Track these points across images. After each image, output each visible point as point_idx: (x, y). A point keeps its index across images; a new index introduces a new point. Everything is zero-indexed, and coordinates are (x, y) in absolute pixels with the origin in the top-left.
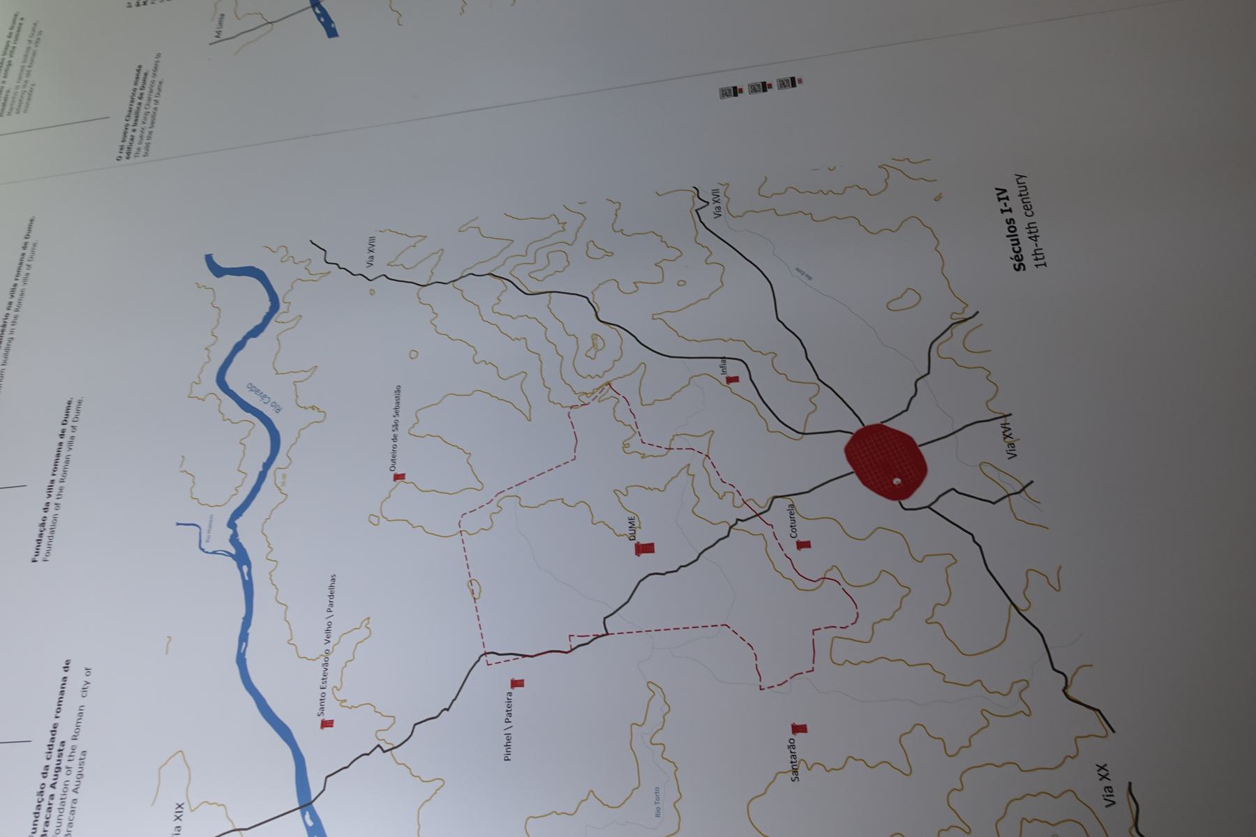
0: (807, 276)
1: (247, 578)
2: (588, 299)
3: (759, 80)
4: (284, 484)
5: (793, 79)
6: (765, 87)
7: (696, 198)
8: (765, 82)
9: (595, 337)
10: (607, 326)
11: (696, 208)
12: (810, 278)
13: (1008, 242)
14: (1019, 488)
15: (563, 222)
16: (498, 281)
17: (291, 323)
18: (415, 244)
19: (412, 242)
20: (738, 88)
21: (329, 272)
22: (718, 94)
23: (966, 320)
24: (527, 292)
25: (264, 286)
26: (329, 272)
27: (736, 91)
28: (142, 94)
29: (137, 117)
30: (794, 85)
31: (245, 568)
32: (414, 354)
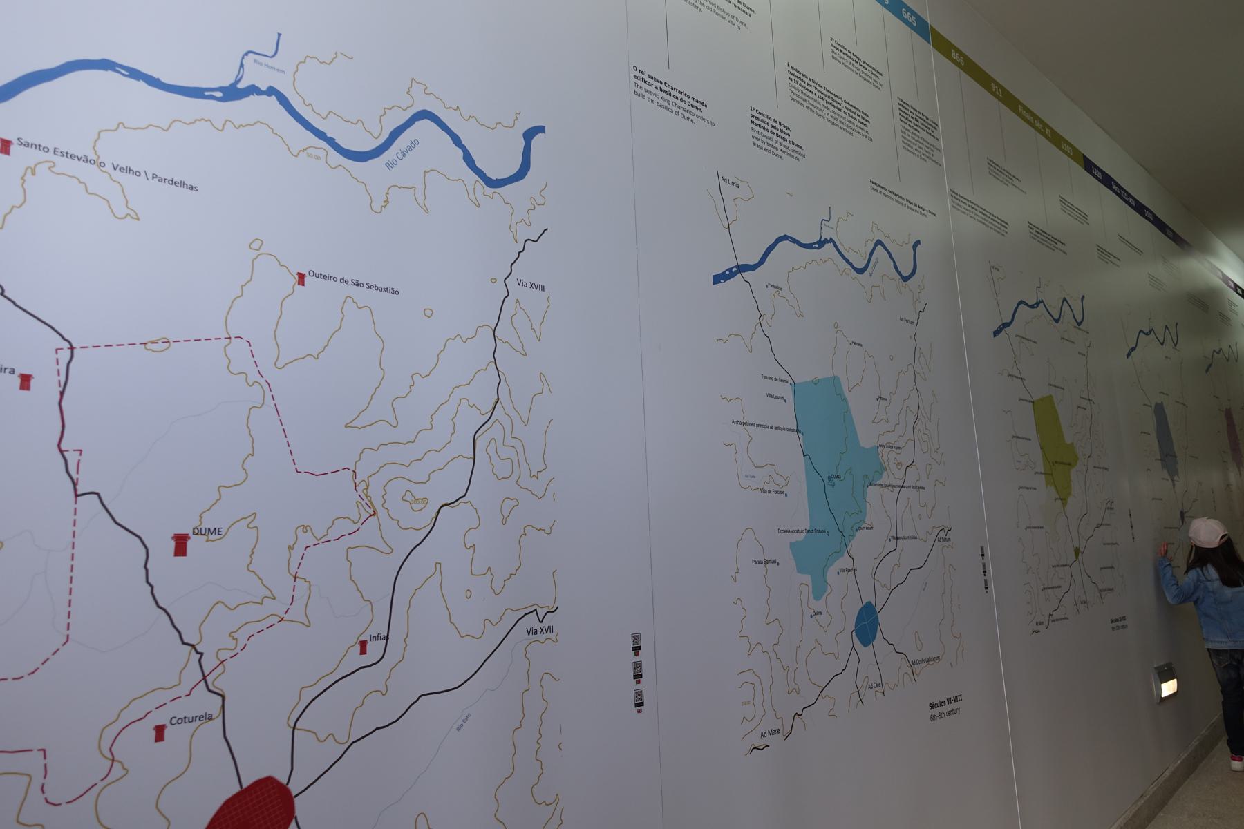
1: (206, 93)
4: (310, 155)
7: (547, 610)
9: (425, 501)
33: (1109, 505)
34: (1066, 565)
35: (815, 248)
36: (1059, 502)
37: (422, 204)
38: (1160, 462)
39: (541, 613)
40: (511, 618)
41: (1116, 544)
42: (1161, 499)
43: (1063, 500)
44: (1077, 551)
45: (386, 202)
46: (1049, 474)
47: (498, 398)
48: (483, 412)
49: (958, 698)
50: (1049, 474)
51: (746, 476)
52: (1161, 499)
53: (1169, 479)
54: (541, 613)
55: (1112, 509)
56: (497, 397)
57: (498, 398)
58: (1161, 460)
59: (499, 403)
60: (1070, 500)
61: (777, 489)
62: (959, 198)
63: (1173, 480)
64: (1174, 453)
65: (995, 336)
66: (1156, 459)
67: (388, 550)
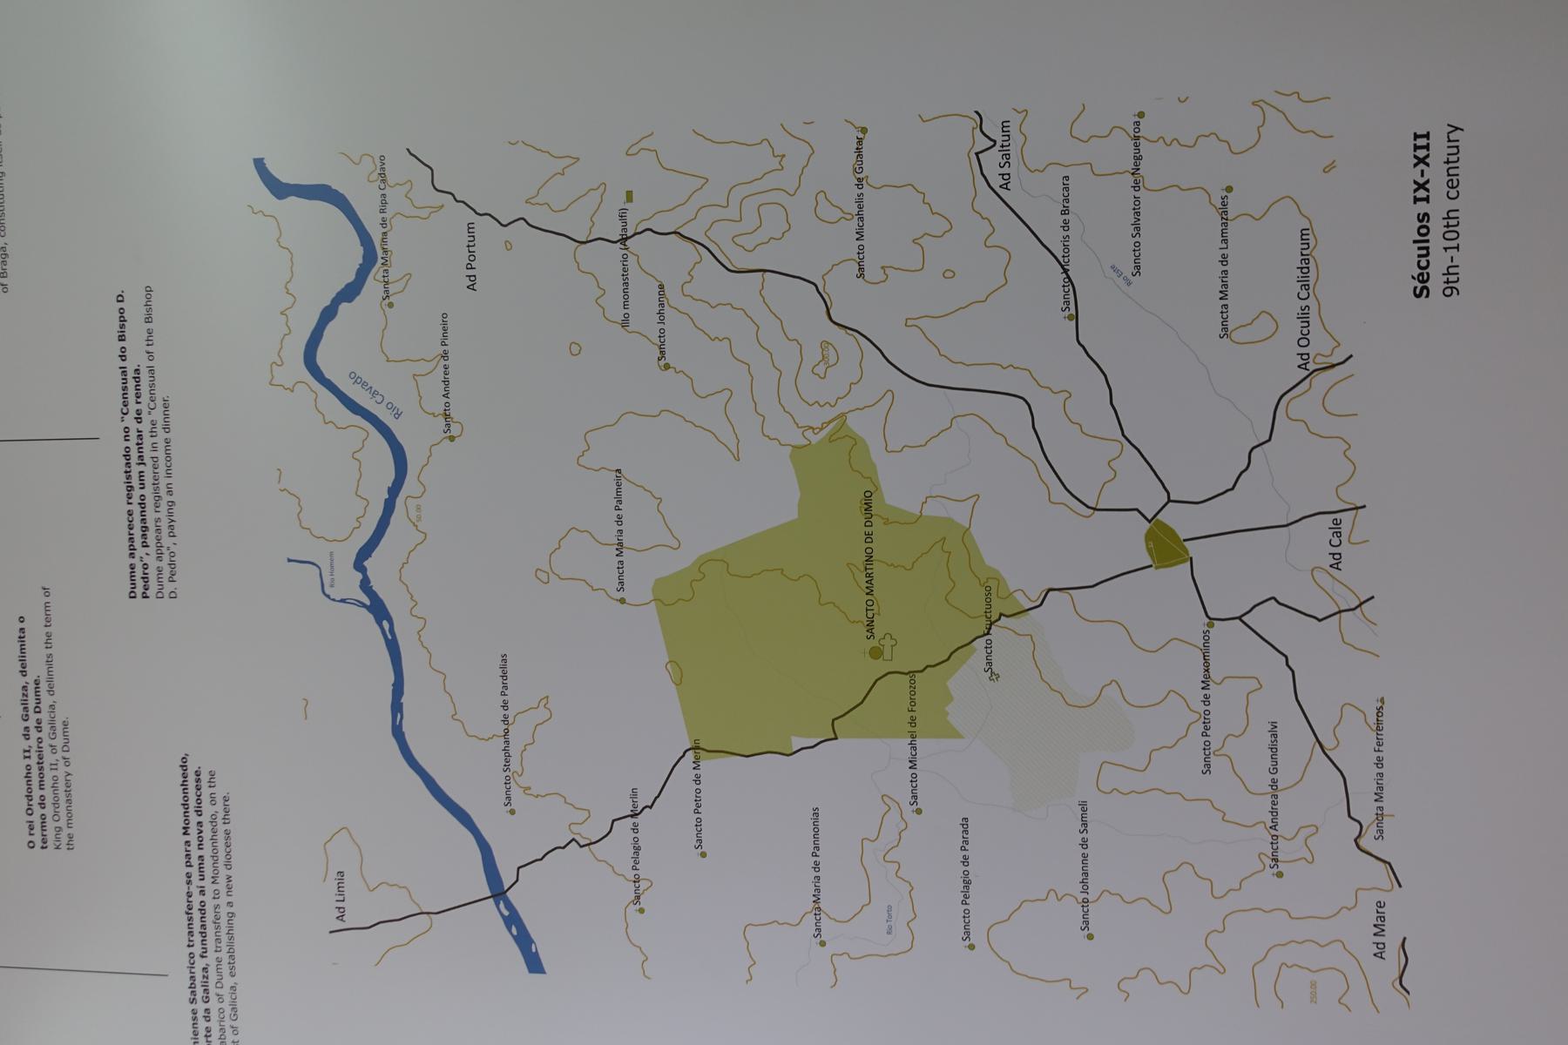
1: (390, 637)
9: (825, 345)
10: (843, 331)
16: (689, 245)
23: (1333, 366)
31: (386, 624)
47: (675, 233)
57: (675, 233)
65: (544, 973)
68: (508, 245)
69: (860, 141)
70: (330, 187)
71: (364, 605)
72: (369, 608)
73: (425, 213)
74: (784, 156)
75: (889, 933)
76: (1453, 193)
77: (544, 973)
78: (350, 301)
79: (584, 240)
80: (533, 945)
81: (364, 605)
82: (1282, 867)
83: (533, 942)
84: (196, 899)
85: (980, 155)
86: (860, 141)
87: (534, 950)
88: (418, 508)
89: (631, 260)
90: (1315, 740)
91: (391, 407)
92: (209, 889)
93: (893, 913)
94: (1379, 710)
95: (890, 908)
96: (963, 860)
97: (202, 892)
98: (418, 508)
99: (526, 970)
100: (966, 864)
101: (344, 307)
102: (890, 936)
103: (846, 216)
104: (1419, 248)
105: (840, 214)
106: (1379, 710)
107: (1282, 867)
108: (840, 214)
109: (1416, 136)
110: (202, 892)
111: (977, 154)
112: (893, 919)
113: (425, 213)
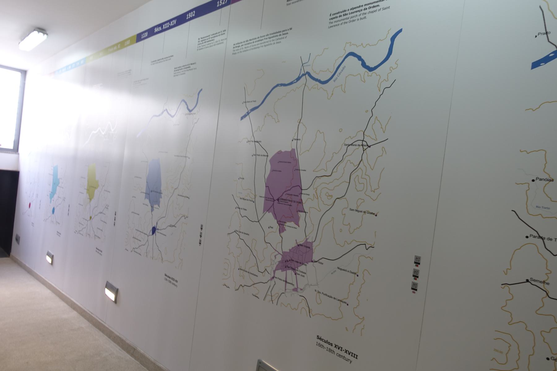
0: (333, 273)
1: (293, 82)
2: (344, 196)
3: (422, 262)
4: (313, 88)
5: (416, 290)
6: (416, 277)
7: (370, 246)
8: (418, 278)
9: (332, 196)
10: (334, 201)
11: (366, 245)
12: (332, 274)
13: (326, 340)
14: (273, 299)
15: (375, 191)
16: (358, 163)
17: (363, 79)
18: (382, 128)
19: (384, 127)
20: (417, 278)
21: (380, 91)
22: (418, 255)
23: (309, 313)
24: (352, 174)
25: (388, 53)
26: (380, 91)
27: (417, 264)
28: (341, 16)
29: (338, 21)
30: (412, 289)
31: (296, 81)
32: (341, 130)
33: (107, 207)
34: (146, 234)
35: (295, 83)
36: (89, 200)
37: (344, 91)
38: (145, 194)
39: (185, 217)
40: (354, 244)
41: (106, 223)
42: (139, 215)
43: (90, 199)
44: (91, 218)
45: (332, 94)
46: (148, 194)
47: (362, 159)
48: (355, 165)
49: (356, 356)
50: (148, 194)
51: (239, 193)
52: (139, 215)
53: (149, 205)
54: (185, 217)
55: (108, 209)
56: (361, 159)
57: (362, 159)
58: (87, 190)
59: (362, 162)
60: (93, 200)
61: (251, 199)
62: (250, 42)
63: (152, 207)
64: (161, 191)
65: (532, 68)
66: (142, 192)
67: (320, 210)
68: (367, 111)
69: (374, 214)
70: (391, 55)
71: (300, 75)
72: (299, 76)
73: (379, 86)
74: (374, 192)
75: (537, 207)
76: (338, 355)
77: (532, 68)
78: (362, 65)
79: (365, 133)
80: (544, 64)
81: (300, 75)
82: (240, 270)
83: (545, 64)
84: (240, 45)
85: (365, 245)
86: (374, 214)
87: (541, 64)
88: (315, 88)
89: (357, 147)
90: (255, 283)
91: (337, 79)
92: (244, 47)
93: (546, 210)
94: (257, 297)
95: (549, 208)
96: (550, 238)
97: (242, 46)
98: (315, 88)
99: (533, 62)
100: (548, 239)
101: (360, 62)
102: (535, 207)
103: (358, 206)
104: (326, 341)
105: (358, 205)
106: (257, 297)
107: (240, 270)
108: (358, 205)
109: (357, 356)
110: (242, 46)
111: (365, 244)
112: (544, 209)
113: (379, 86)
